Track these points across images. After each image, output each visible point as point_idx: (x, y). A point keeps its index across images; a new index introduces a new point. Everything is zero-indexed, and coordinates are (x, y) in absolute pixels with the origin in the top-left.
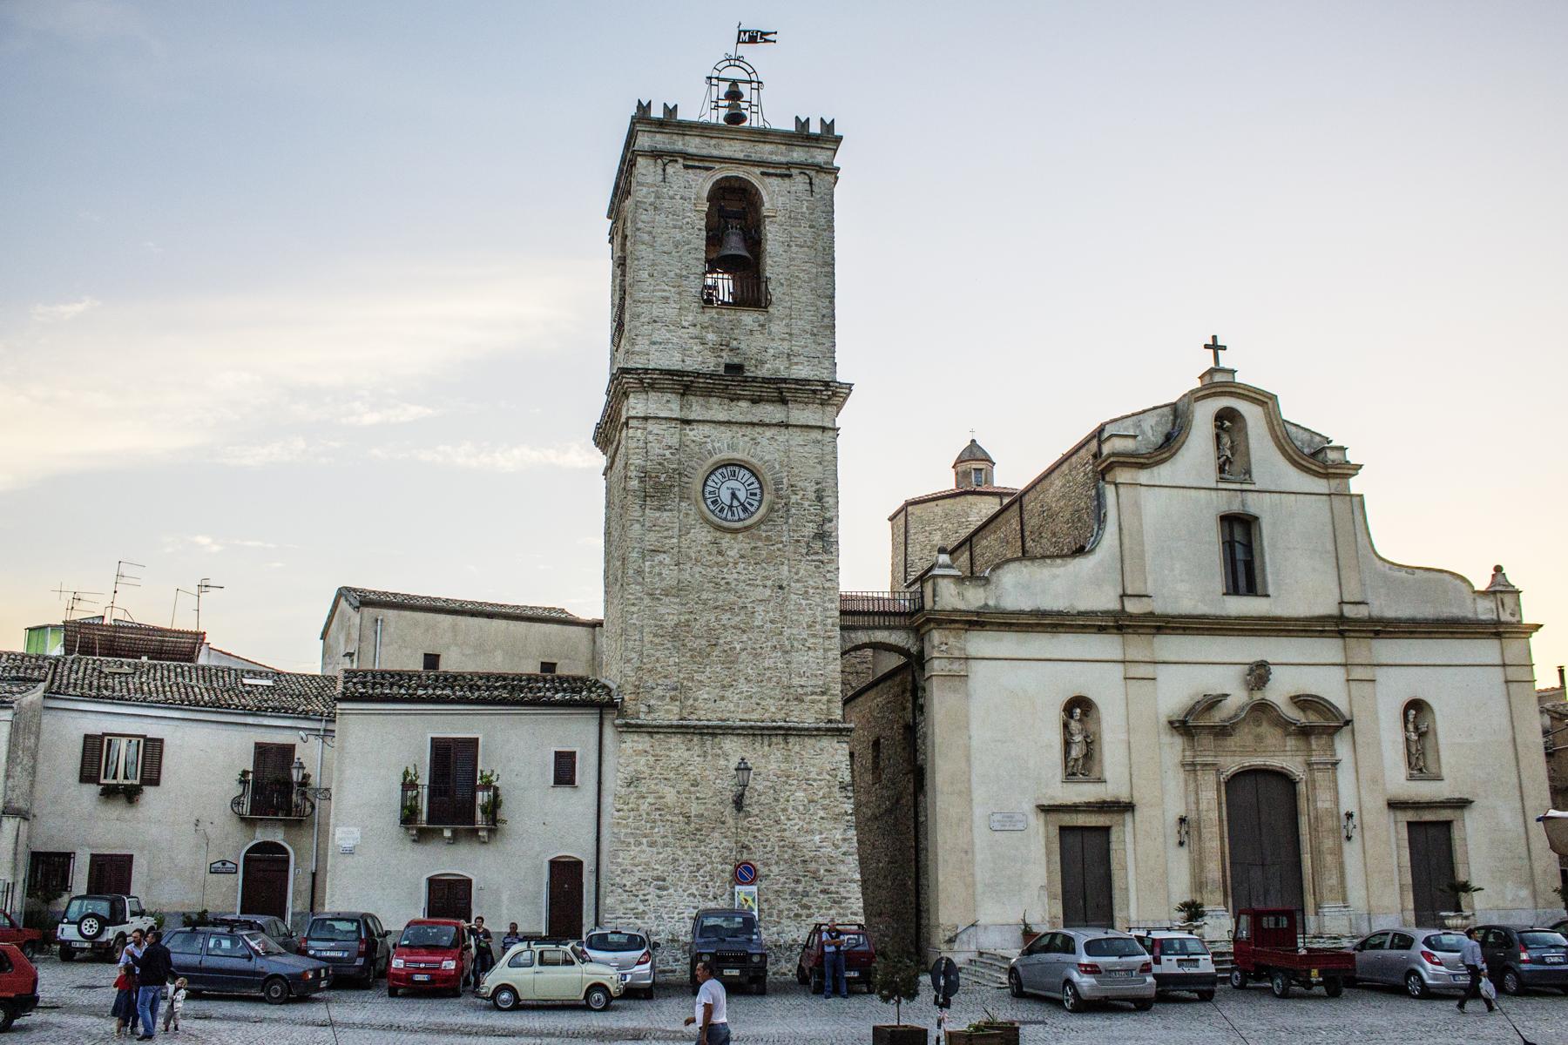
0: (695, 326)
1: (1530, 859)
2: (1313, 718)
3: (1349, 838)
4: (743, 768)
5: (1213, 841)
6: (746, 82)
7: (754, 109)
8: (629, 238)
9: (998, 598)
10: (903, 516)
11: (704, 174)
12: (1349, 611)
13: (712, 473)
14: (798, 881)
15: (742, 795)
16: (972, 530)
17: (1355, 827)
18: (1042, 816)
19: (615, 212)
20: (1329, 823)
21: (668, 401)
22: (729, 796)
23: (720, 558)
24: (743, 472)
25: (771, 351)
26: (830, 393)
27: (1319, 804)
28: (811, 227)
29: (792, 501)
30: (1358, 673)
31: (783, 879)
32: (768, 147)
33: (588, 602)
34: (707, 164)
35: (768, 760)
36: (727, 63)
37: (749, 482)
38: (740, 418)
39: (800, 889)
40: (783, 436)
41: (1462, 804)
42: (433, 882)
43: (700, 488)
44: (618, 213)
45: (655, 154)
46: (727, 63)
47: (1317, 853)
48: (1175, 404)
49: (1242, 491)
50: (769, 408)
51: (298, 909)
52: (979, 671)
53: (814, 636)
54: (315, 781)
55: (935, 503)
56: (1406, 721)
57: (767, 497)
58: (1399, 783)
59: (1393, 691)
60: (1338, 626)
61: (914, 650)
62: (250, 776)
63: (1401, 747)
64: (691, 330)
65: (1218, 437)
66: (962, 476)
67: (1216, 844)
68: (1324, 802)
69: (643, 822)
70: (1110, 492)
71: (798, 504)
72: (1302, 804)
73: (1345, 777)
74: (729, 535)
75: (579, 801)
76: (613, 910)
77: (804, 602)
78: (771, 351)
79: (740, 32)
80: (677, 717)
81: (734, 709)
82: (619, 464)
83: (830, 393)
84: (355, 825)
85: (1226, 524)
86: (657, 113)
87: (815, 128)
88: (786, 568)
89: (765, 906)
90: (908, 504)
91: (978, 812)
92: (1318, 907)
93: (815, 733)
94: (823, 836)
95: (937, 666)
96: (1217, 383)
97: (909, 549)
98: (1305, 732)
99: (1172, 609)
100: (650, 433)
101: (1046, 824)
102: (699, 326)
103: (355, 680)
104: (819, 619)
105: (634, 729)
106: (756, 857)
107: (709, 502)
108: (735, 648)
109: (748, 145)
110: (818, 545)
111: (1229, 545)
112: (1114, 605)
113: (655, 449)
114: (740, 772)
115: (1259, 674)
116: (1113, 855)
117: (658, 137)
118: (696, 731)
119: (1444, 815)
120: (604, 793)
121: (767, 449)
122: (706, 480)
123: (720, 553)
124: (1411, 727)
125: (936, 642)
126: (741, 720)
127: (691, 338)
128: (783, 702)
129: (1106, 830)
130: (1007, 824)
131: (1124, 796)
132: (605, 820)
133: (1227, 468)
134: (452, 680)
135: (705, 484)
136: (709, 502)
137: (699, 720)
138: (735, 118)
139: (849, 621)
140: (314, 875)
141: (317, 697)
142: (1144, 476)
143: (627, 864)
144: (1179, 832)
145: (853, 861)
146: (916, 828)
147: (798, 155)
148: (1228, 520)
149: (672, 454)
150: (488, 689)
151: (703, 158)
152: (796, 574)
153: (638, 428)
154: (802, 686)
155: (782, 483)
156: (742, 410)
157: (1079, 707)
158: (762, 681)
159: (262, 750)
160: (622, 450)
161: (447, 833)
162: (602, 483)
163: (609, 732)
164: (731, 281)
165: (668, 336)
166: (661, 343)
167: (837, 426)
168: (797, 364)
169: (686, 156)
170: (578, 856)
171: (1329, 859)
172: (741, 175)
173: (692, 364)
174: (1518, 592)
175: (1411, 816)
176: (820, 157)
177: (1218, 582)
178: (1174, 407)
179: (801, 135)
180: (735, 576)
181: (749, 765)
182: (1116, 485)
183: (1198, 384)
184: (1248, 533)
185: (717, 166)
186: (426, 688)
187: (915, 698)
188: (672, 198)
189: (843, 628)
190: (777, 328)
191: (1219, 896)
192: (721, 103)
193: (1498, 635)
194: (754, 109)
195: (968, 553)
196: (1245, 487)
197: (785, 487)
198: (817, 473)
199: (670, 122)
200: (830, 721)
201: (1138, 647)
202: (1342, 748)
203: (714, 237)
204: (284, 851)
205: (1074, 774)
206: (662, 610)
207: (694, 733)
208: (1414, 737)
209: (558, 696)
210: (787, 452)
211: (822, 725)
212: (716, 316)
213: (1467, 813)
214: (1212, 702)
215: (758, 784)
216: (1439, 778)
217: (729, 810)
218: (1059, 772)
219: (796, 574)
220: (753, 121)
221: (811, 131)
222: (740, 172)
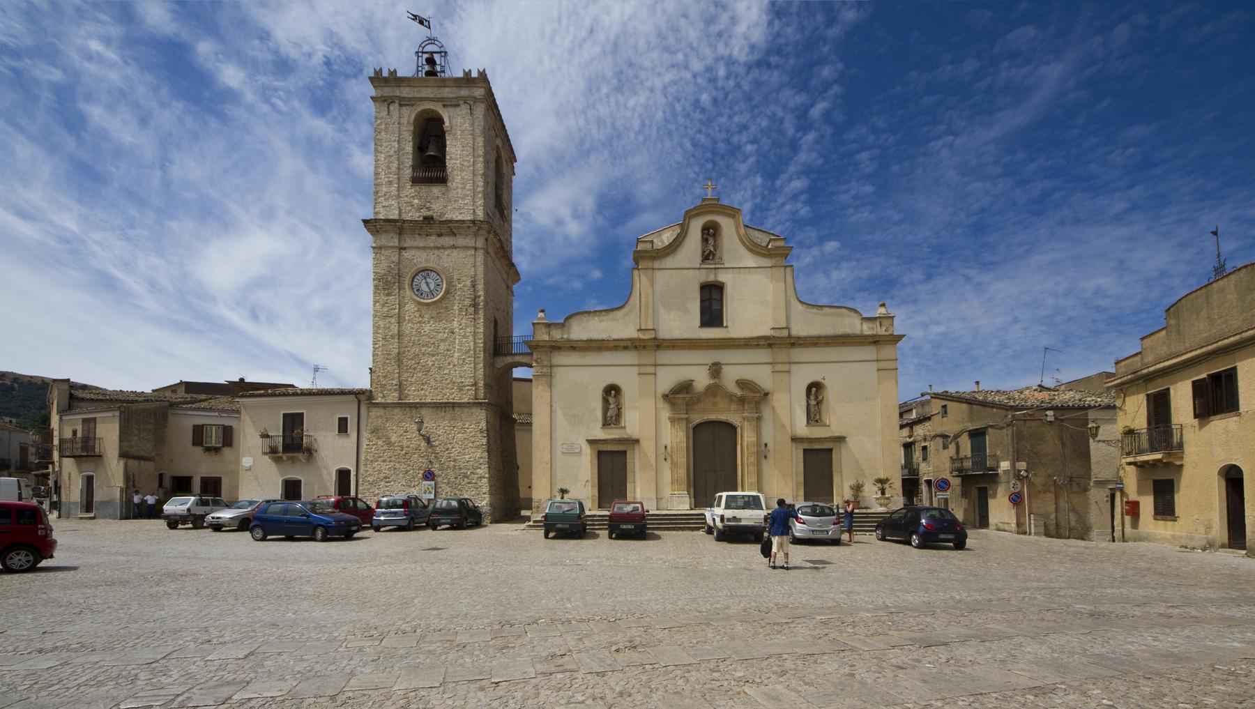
21: (392, 238)
24: (433, 273)
38: (432, 245)
49: (715, 268)
58: (801, 427)
59: (802, 377)
60: (767, 343)
64: (405, 198)
115: (716, 369)
117: (386, 89)
136: (415, 290)
142: (657, 264)
156: (432, 241)
169: (400, 99)
170: (350, 468)
183: (238, 380)
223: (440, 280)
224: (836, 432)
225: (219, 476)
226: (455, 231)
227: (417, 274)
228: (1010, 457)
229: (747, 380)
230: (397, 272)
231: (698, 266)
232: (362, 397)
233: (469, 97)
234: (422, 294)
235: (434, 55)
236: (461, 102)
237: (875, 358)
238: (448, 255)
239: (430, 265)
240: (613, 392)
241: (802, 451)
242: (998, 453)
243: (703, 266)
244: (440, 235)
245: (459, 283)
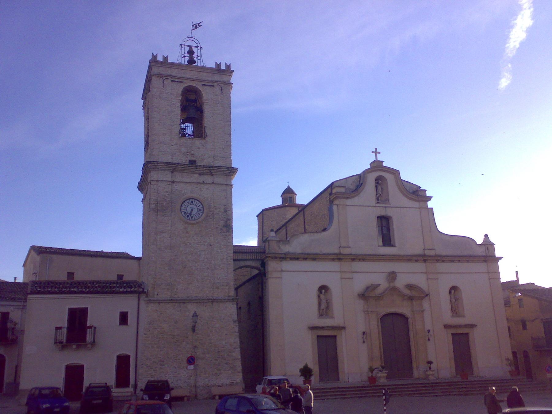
0: (177, 145)
2: (414, 293)
3: (429, 340)
4: (195, 315)
6: (195, 47)
7: (199, 58)
8: (150, 109)
10: (263, 215)
11: (179, 84)
12: (427, 253)
13: (184, 202)
15: (195, 326)
16: (287, 220)
17: (431, 336)
19: (144, 97)
21: (167, 174)
23: (187, 235)
24: (196, 201)
25: (207, 155)
26: (231, 171)
28: (222, 107)
29: (215, 212)
32: (205, 74)
33: (136, 251)
34: (181, 80)
35: (204, 312)
36: (188, 39)
37: (198, 205)
38: (195, 181)
41: (473, 326)
43: (179, 207)
44: (145, 98)
45: (160, 76)
46: (188, 39)
48: (360, 174)
49: (386, 207)
50: (206, 177)
54: (18, 327)
55: (273, 210)
57: (205, 211)
58: (449, 319)
60: (423, 258)
63: (449, 305)
64: (175, 147)
65: (376, 187)
66: (284, 200)
69: (155, 339)
70: (335, 207)
71: (217, 214)
72: (411, 326)
73: (427, 315)
74: (190, 226)
77: (219, 251)
78: (207, 155)
79: (192, 25)
80: (170, 297)
82: (148, 196)
83: (229, 171)
85: (380, 219)
86: (160, 58)
88: (213, 238)
90: (264, 210)
93: (223, 301)
94: (227, 341)
96: (377, 165)
97: (264, 228)
98: (411, 298)
99: (358, 252)
100: (160, 186)
102: (178, 145)
103: (36, 285)
104: (225, 257)
105: (152, 302)
107: (183, 213)
108: (193, 269)
109: (197, 73)
110: (225, 229)
112: (337, 251)
114: (194, 317)
115: (392, 276)
118: (177, 302)
122: (182, 205)
123: (187, 232)
124: (452, 296)
126: (195, 297)
127: (175, 150)
128: (212, 289)
131: (342, 325)
132: (140, 338)
133: (380, 198)
134: (79, 284)
135: (181, 206)
136: (183, 213)
137: (178, 297)
138: (191, 61)
139: (240, 257)
140: (16, 367)
141: (20, 292)
142: (348, 202)
144: (363, 337)
145: (238, 350)
147: (217, 77)
148: (380, 218)
149: (168, 195)
150: (92, 288)
151: (179, 78)
152: (217, 240)
153: (154, 185)
154: (219, 283)
155: (211, 206)
156: (195, 178)
158: (203, 281)
160: (148, 193)
161: (74, 346)
162: (141, 205)
163: (142, 303)
164: (192, 128)
166: (163, 152)
167: (232, 184)
168: (217, 160)
169: (172, 77)
170: (129, 354)
172: (194, 85)
174: (296, 195)
176: (225, 78)
178: (359, 176)
179: (218, 69)
180: (193, 241)
181: (198, 314)
182: (337, 205)
183: (369, 167)
185: (185, 81)
188: (167, 94)
189: (234, 260)
192: (186, 55)
193: (486, 261)
195: (285, 230)
196: (386, 205)
197: (212, 207)
199: (165, 62)
201: (346, 266)
202: (426, 304)
203: (184, 109)
205: (322, 315)
207: (176, 302)
208: (454, 300)
209: (121, 290)
211: (226, 298)
212: (185, 141)
214: (374, 287)
216: (464, 316)
219: (217, 240)
220: (198, 63)
221: (222, 68)
222: (193, 84)
223: (201, 206)
227: (184, 202)
229: (415, 285)
230: (169, 199)
231: (375, 205)
236: (215, 84)
238: (207, 189)
239: (195, 196)
240: (323, 291)
241: (451, 334)
245: (216, 209)
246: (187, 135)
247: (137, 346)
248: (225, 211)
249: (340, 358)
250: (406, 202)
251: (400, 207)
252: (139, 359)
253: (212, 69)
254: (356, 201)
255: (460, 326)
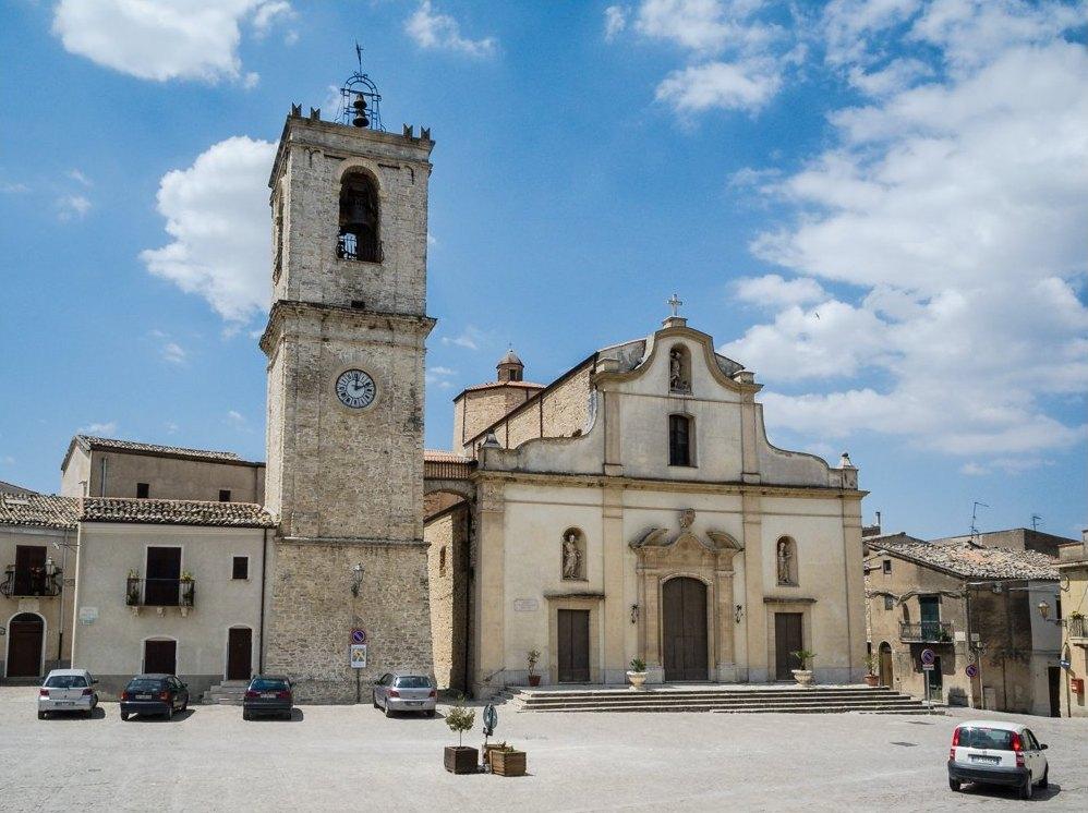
1: (849, 637)
5: (654, 621)
7: (374, 116)
9: (525, 464)
12: (747, 478)
14: (392, 642)
18: (547, 602)
20: (726, 612)
22: (349, 588)
27: (721, 600)
30: (750, 518)
31: (383, 640)
35: (376, 564)
36: (355, 79)
39: (394, 646)
40: (390, 351)
42: (149, 644)
46: (355, 79)
47: (718, 629)
49: (685, 399)
51: (50, 658)
52: (512, 509)
53: (408, 485)
56: (779, 550)
58: (771, 586)
59: (772, 530)
60: (740, 485)
61: (470, 495)
62: (14, 569)
65: (672, 363)
67: (655, 623)
68: (724, 599)
72: (710, 601)
75: (249, 590)
76: (271, 661)
81: (354, 528)
84: (94, 606)
86: (306, 114)
87: (417, 134)
89: (371, 658)
91: (508, 599)
92: (717, 664)
95: (485, 505)
101: (550, 607)
106: (367, 625)
111: (673, 433)
113: (304, 356)
115: (687, 516)
116: (591, 628)
117: (307, 132)
119: (797, 609)
120: (267, 585)
121: (381, 360)
124: (781, 553)
125: (485, 491)
129: (587, 612)
130: (524, 604)
132: (268, 602)
138: (361, 123)
141: (60, 513)
142: (623, 387)
143: (281, 631)
146: (468, 607)
157: (573, 534)
159: (23, 552)
165: (314, 278)
169: (327, 148)
170: (249, 626)
171: (725, 635)
173: (329, 299)
175: (777, 609)
176: (421, 155)
177: (665, 458)
180: (356, 444)
184: (686, 428)
186: (143, 513)
187: (470, 523)
188: (316, 179)
190: (388, 277)
191: (655, 656)
194: (374, 116)
198: (411, 378)
200: (415, 540)
204: (41, 619)
206: (307, 465)
208: (782, 560)
209: (236, 521)
210: (392, 363)
213: (813, 606)
215: (369, 580)
217: (351, 594)
218: (559, 574)
221: (414, 136)
224: (593, 584)
225: (143, 645)
226: (394, 325)
228: (966, 628)
231: (666, 393)
232: (271, 533)
233: (409, 159)
234: (348, 400)
235: (365, 97)
236: (402, 165)
237: (600, 502)
239: (359, 366)
242: (953, 622)
243: (671, 395)
244: (372, 328)
246: (345, 256)
247: (262, 615)
248: (413, 394)
249: (593, 645)
250: (718, 391)
251: (709, 401)
252: (265, 634)
253: (398, 136)
254: (636, 385)
255: (790, 601)
